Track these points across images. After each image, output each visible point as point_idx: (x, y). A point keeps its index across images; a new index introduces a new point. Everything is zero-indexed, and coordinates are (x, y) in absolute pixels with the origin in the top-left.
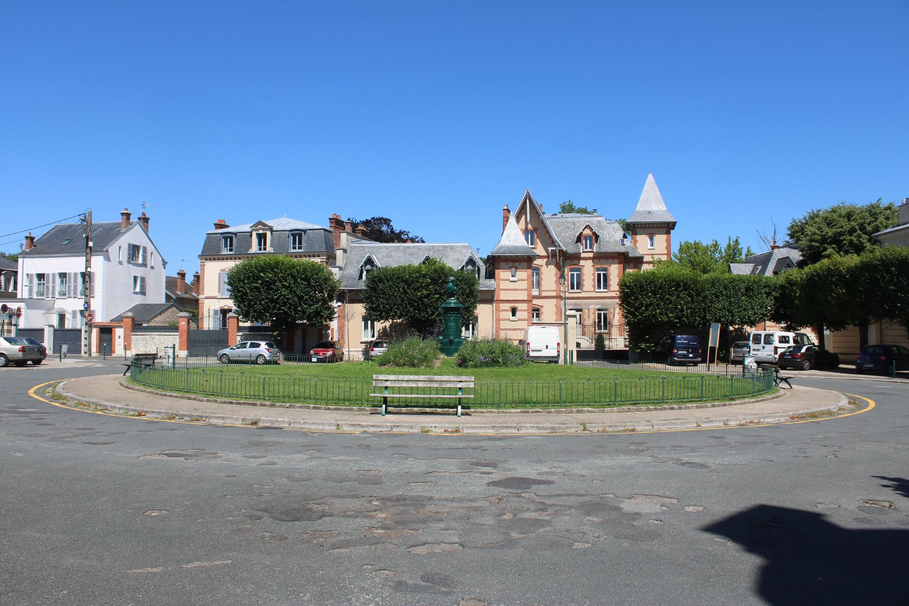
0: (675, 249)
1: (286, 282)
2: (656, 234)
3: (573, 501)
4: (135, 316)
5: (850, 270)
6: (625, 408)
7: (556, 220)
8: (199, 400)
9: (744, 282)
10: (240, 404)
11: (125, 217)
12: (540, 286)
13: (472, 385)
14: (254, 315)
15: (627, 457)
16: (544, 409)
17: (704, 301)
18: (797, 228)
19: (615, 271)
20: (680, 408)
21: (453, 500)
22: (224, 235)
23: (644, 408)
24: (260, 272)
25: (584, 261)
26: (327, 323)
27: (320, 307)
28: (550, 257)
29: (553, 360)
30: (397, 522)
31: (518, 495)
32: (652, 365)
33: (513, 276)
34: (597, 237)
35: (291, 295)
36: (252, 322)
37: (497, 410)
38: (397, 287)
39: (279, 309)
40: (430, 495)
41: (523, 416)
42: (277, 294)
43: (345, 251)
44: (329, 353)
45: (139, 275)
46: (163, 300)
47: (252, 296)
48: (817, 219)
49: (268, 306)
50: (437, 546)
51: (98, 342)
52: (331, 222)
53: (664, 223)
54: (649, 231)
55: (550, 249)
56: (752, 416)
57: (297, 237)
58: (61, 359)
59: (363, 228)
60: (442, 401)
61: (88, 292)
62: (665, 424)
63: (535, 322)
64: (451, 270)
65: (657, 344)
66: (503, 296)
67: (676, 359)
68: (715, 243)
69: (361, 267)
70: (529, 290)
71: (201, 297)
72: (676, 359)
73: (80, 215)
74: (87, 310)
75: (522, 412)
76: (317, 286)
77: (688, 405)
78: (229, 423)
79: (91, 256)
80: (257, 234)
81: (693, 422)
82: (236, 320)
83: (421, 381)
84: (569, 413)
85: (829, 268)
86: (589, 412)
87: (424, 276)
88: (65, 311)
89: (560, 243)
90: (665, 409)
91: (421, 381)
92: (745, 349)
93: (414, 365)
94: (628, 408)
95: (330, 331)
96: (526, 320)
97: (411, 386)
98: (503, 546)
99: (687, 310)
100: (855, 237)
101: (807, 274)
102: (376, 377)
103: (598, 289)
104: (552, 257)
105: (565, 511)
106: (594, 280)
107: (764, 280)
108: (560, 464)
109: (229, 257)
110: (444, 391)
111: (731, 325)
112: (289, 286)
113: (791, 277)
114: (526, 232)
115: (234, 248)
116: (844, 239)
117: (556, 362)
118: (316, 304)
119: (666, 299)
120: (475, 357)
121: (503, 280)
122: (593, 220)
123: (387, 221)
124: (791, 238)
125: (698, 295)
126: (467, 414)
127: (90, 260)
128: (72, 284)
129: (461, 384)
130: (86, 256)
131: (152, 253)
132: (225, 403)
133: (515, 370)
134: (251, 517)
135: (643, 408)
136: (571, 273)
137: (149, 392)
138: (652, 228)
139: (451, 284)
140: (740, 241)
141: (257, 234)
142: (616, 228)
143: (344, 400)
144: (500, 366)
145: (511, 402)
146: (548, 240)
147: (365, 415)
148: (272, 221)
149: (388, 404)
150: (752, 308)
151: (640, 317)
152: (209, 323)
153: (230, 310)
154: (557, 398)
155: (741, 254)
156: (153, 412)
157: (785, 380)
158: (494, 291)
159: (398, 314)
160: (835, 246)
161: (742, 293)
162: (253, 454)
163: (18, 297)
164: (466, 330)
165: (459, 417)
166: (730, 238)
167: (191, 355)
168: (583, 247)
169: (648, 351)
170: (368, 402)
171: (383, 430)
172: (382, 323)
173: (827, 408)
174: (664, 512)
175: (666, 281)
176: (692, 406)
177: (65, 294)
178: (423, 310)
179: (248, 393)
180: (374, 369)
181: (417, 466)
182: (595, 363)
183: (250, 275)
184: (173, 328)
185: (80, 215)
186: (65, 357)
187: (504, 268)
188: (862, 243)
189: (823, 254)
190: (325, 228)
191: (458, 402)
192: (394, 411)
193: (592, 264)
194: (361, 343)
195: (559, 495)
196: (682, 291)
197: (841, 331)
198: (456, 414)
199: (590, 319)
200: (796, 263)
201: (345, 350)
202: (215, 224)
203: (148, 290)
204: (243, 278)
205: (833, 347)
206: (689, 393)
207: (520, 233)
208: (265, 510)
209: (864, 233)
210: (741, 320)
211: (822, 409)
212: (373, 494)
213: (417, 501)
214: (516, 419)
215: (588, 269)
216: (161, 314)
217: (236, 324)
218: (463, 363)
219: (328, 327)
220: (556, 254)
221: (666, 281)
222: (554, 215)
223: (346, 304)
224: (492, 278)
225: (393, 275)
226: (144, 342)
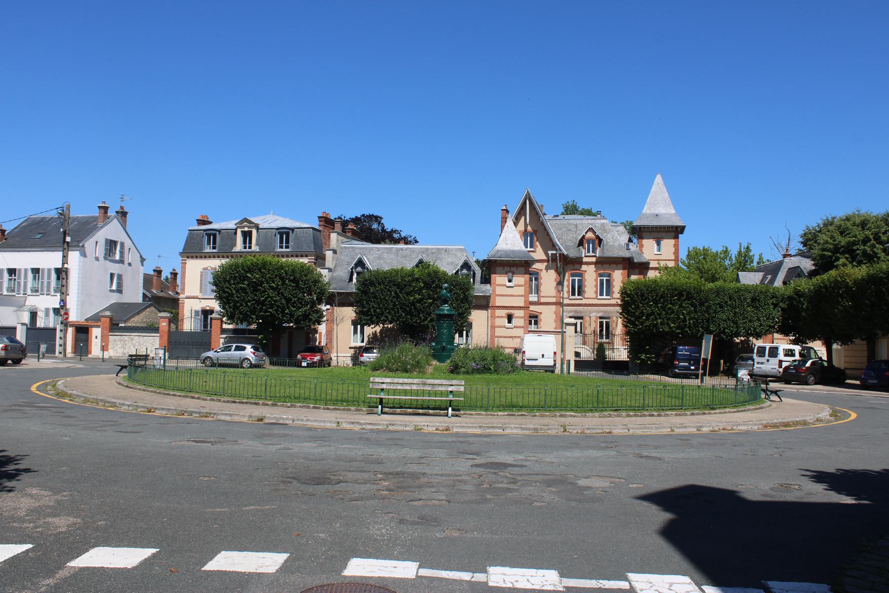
0: (683, 255)
1: (274, 283)
2: (663, 238)
3: (540, 477)
4: (113, 316)
5: (856, 282)
6: (606, 413)
7: (557, 222)
8: (203, 399)
9: (750, 292)
10: (243, 403)
11: (103, 211)
12: (539, 292)
13: (462, 389)
14: (239, 317)
15: (595, 451)
16: (530, 413)
17: (707, 312)
18: (810, 236)
19: (618, 277)
20: (659, 415)
21: (442, 475)
23: (624, 414)
24: (247, 272)
25: (586, 266)
26: (316, 326)
27: (308, 310)
28: (550, 262)
29: (550, 369)
30: (398, 487)
31: (495, 473)
32: (652, 377)
33: (510, 281)
34: (600, 240)
35: (279, 297)
36: (237, 324)
37: (485, 413)
38: (389, 291)
39: (266, 311)
40: (423, 471)
41: (509, 418)
42: (264, 295)
43: (335, 252)
44: (317, 358)
45: (116, 272)
46: (140, 299)
47: (238, 297)
48: (830, 228)
49: (255, 308)
50: (429, 501)
51: (74, 342)
52: (320, 221)
53: (672, 227)
54: (656, 235)
55: (550, 252)
56: (725, 424)
57: (284, 236)
58: (39, 360)
59: (353, 227)
60: (434, 403)
61: (64, 289)
62: (641, 428)
63: (533, 329)
64: (445, 274)
65: (658, 356)
67: (677, 370)
68: (725, 250)
69: (352, 269)
70: (526, 296)
71: (181, 296)
72: (677, 370)
73: (57, 208)
74: (62, 309)
75: (508, 415)
76: (306, 288)
77: (667, 413)
78: (236, 419)
79: (68, 251)
80: (242, 231)
81: (668, 428)
82: (220, 321)
83: (414, 384)
84: (552, 417)
85: (836, 280)
86: (571, 416)
87: (417, 280)
88: (37, 309)
89: (561, 247)
90: (645, 416)
91: (414, 384)
92: (750, 362)
93: (406, 371)
94: (609, 414)
95: (317, 335)
96: (522, 327)
97: (405, 388)
98: (478, 503)
99: (689, 320)
100: (869, 247)
101: (814, 285)
102: (373, 380)
103: (600, 295)
104: (552, 261)
105: (531, 484)
106: (596, 286)
107: (771, 291)
108: (536, 455)
109: (211, 255)
110: (436, 394)
111: (737, 337)
112: (277, 288)
113: (799, 288)
114: (525, 234)
115: (217, 246)
116: (858, 249)
117: (553, 372)
118: (305, 307)
119: (668, 308)
120: (467, 364)
121: (499, 285)
122: (596, 223)
123: (377, 219)
124: (804, 246)
125: (702, 304)
126: (457, 416)
127: (68, 256)
128: (46, 281)
129: (452, 387)
130: (63, 252)
131: (130, 249)
132: (228, 402)
133: (506, 377)
134: (283, 482)
135: (623, 414)
136: (573, 278)
137: (152, 391)
138: (659, 232)
139: (445, 291)
140: (751, 248)
141: (242, 231)
142: (621, 232)
143: (342, 401)
144: (491, 373)
145: (499, 406)
146: (549, 243)
147: (362, 414)
148: (257, 218)
149: (384, 405)
150: (758, 319)
151: (641, 327)
152: (189, 325)
153: (212, 312)
154: (542, 403)
155: (753, 261)
156: (163, 409)
157: (775, 392)
158: (490, 296)
159: (390, 319)
160: (847, 256)
161: (748, 303)
162: (268, 442)
164: (459, 336)
165: (449, 418)
166: (740, 244)
168: (585, 251)
169: (649, 362)
170: (364, 403)
171: (379, 428)
172: (372, 328)
173: (803, 419)
174: (610, 487)
175: (668, 290)
176: (671, 414)
177: (37, 291)
178: (415, 315)
179: (250, 393)
180: (368, 373)
181: (414, 453)
183: (236, 275)
184: (152, 329)
185: (57, 208)
186: (44, 357)
187: (500, 273)
188: (876, 254)
189: (835, 264)
190: (314, 226)
191: (448, 405)
192: (389, 412)
193: (595, 269)
194: (350, 348)
195: (529, 474)
196: (684, 300)
197: (848, 345)
198: (447, 416)
199: (592, 325)
200: (808, 273)
201: (333, 356)
202: (197, 220)
203: (124, 288)
204: (229, 278)
205: (845, 362)
206: (674, 402)
207: (518, 236)
208: (294, 478)
209: (878, 243)
210: (747, 331)
211: (797, 419)
212: (378, 470)
213: (413, 475)
214: (502, 421)
215: (590, 274)
216: (138, 313)
217: (219, 326)
218: (455, 370)
219: (316, 331)
220: (557, 258)
221: (668, 290)
222: (555, 216)
223: (335, 308)
224: (488, 283)
225: (385, 278)
226: (123, 342)
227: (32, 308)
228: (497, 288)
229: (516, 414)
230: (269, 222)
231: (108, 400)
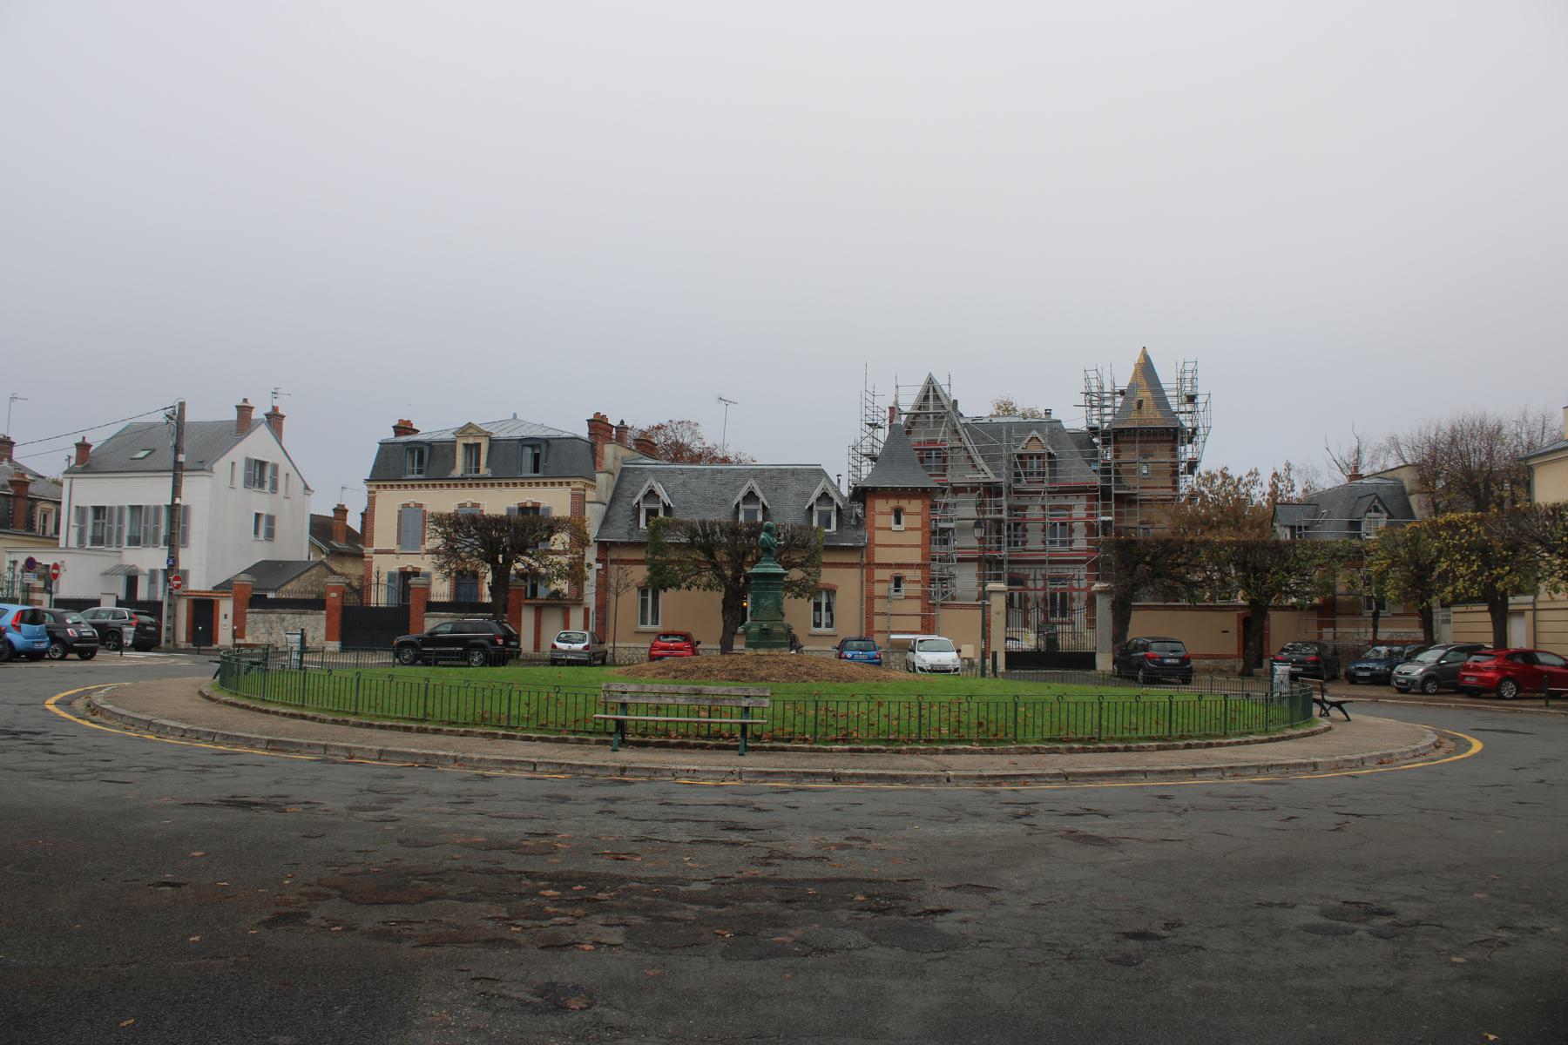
22: (409, 446)
66: (881, 556)
73: (166, 408)
88: (137, 571)
102: (605, 687)
129: (748, 700)
131: (287, 475)
163: (60, 546)
167: (345, 648)
182: (1079, 674)
185: (166, 408)
226: (268, 625)
227: (129, 572)
228: (877, 532)
230: (509, 430)
231: (155, 721)
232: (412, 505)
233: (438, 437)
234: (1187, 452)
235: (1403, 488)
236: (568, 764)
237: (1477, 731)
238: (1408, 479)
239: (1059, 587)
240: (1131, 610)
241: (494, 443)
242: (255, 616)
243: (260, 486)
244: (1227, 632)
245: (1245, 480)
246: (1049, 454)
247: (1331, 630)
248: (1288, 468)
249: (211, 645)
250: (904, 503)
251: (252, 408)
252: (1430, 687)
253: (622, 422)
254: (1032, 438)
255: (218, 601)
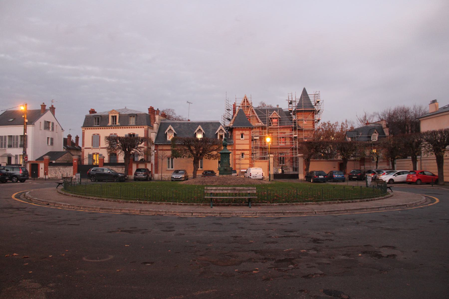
13: (255, 192)
22: (130, 115)
66: (237, 147)
75: (279, 205)
88: (11, 155)
94: (330, 202)
102: (206, 188)
110: (239, 195)
137: (79, 197)
226: (55, 171)
229: (283, 204)
231: (57, 203)
232: (96, 134)
233: (103, 114)
234: (317, 117)
235: (382, 127)
236: (203, 212)
237: (436, 194)
238: (384, 124)
239: (282, 155)
240: (310, 162)
241: (120, 116)
242: (51, 168)
243: (48, 129)
244: (335, 167)
245: (335, 124)
246: (279, 118)
247: (363, 166)
248: (346, 121)
249: (37, 177)
250: (244, 132)
251: (46, 106)
252: (419, 182)
253: (158, 109)
254: (274, 113)
255: (39, 164)
